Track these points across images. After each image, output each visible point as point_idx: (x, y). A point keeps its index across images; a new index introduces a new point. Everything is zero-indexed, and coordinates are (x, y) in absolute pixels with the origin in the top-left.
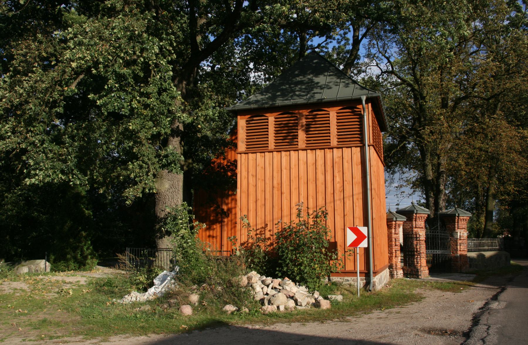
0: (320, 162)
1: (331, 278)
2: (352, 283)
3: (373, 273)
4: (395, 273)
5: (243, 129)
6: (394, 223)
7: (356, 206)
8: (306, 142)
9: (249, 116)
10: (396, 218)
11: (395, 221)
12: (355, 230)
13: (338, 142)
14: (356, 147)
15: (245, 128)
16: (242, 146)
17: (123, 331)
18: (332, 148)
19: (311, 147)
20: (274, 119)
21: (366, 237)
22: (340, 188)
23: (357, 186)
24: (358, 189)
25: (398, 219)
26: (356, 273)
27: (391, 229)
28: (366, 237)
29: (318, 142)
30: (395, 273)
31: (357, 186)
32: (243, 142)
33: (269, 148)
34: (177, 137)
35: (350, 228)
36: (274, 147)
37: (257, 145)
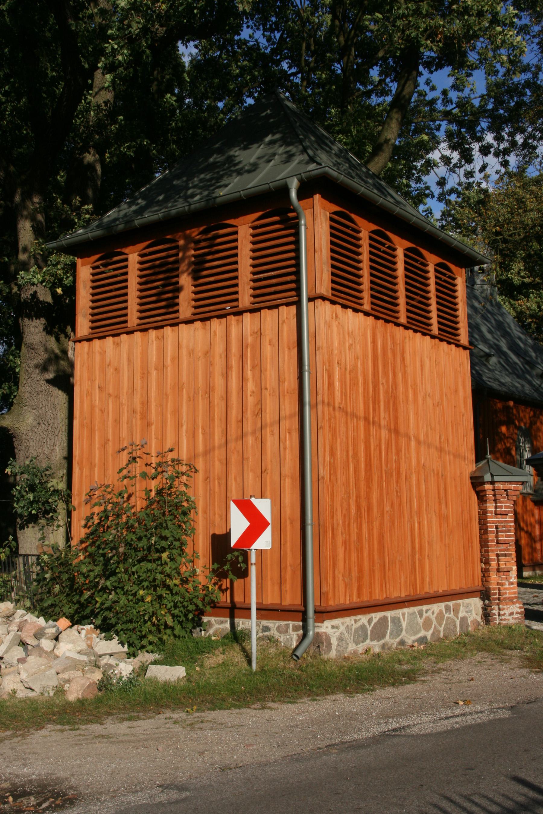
0: (219, 348)
1: (236, 620)
2: (276, 635)
3: (316, 612)
4: (496, 612)
5: (85, 287)
6: (488, 487)
7: (285, 449)
8: (193, 303)
9: (97, 256)
10: (492, 476)
11: (492, 483)
12: (247, 508)
13: (255, 296)
14: (288, 304)
15: (90, 284)
16: (83, 325)
17: (31, 705)
18: (239, 313)
19: (202, 316)
20: (138, 259)
21: (267, 524)
22: (256, 405)
23: (287, 398)
24: (290, 406)
25: (496, 479)
26: (249, 609)
27: (485, 501)
28: (267, 524)
29: (216, 305)
30: (496, 612)
31: (287, 398)
32: (84, 316)
33: (129, 324)
34: (38, 317)
35: (237, 502)
36: (139, 321)
37: (110, 323)
